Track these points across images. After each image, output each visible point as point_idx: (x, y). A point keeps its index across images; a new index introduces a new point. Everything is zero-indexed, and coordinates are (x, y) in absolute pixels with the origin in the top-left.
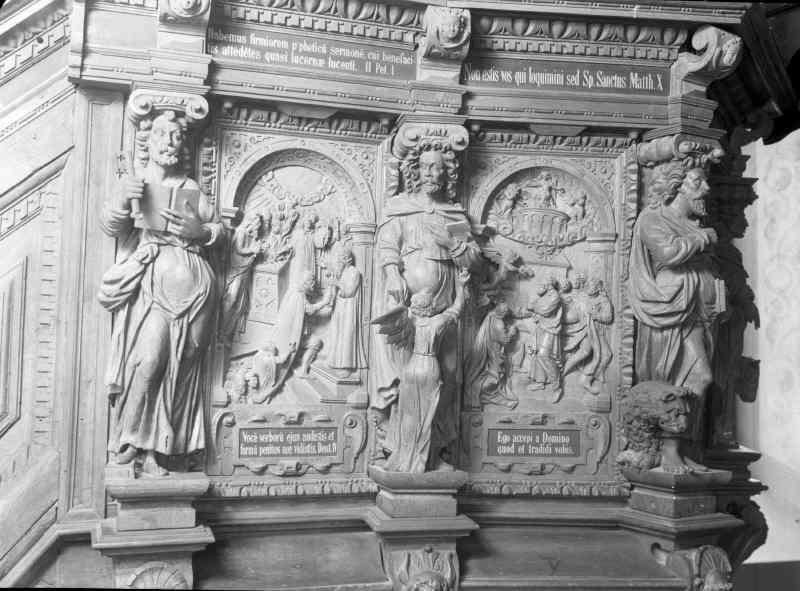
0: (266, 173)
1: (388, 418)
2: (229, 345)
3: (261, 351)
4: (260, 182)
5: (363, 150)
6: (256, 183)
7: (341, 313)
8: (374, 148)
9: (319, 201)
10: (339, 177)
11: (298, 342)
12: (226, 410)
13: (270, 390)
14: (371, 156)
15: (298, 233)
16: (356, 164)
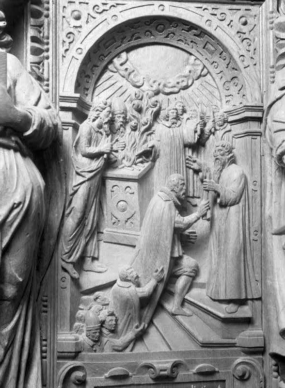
0: (118, 55)
1: (202, 347)
2: (76, 276)
3: (119, 282)
4: (110, 67)
5: (240, 13)
6: (106, 68)
7: (223, 227)
8: (255, 9)
9: (186, 88)
10: (212, 53)
11: (166, 267)
12: (77, 363)
13: (130, 335)
14: (250, 21)
15: (160, 128)
16: (233, 32)
